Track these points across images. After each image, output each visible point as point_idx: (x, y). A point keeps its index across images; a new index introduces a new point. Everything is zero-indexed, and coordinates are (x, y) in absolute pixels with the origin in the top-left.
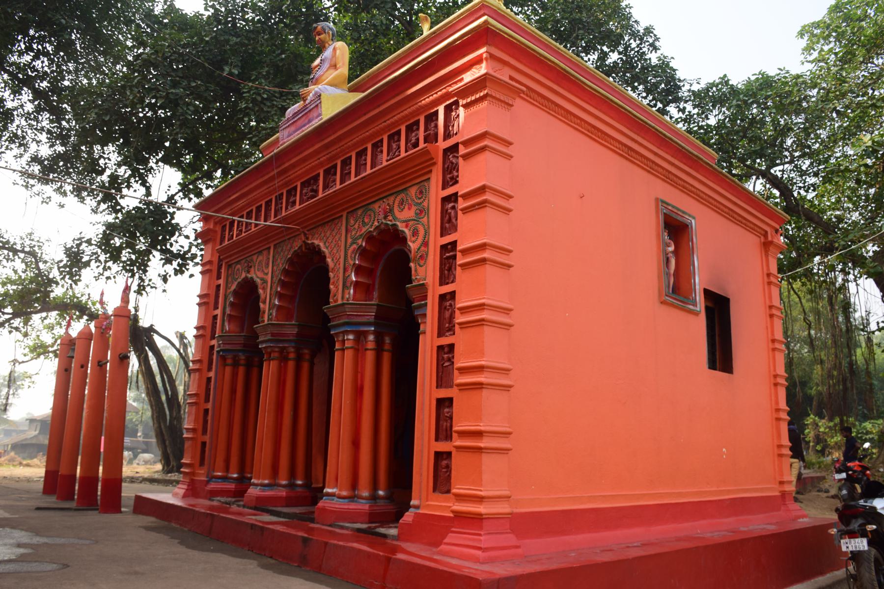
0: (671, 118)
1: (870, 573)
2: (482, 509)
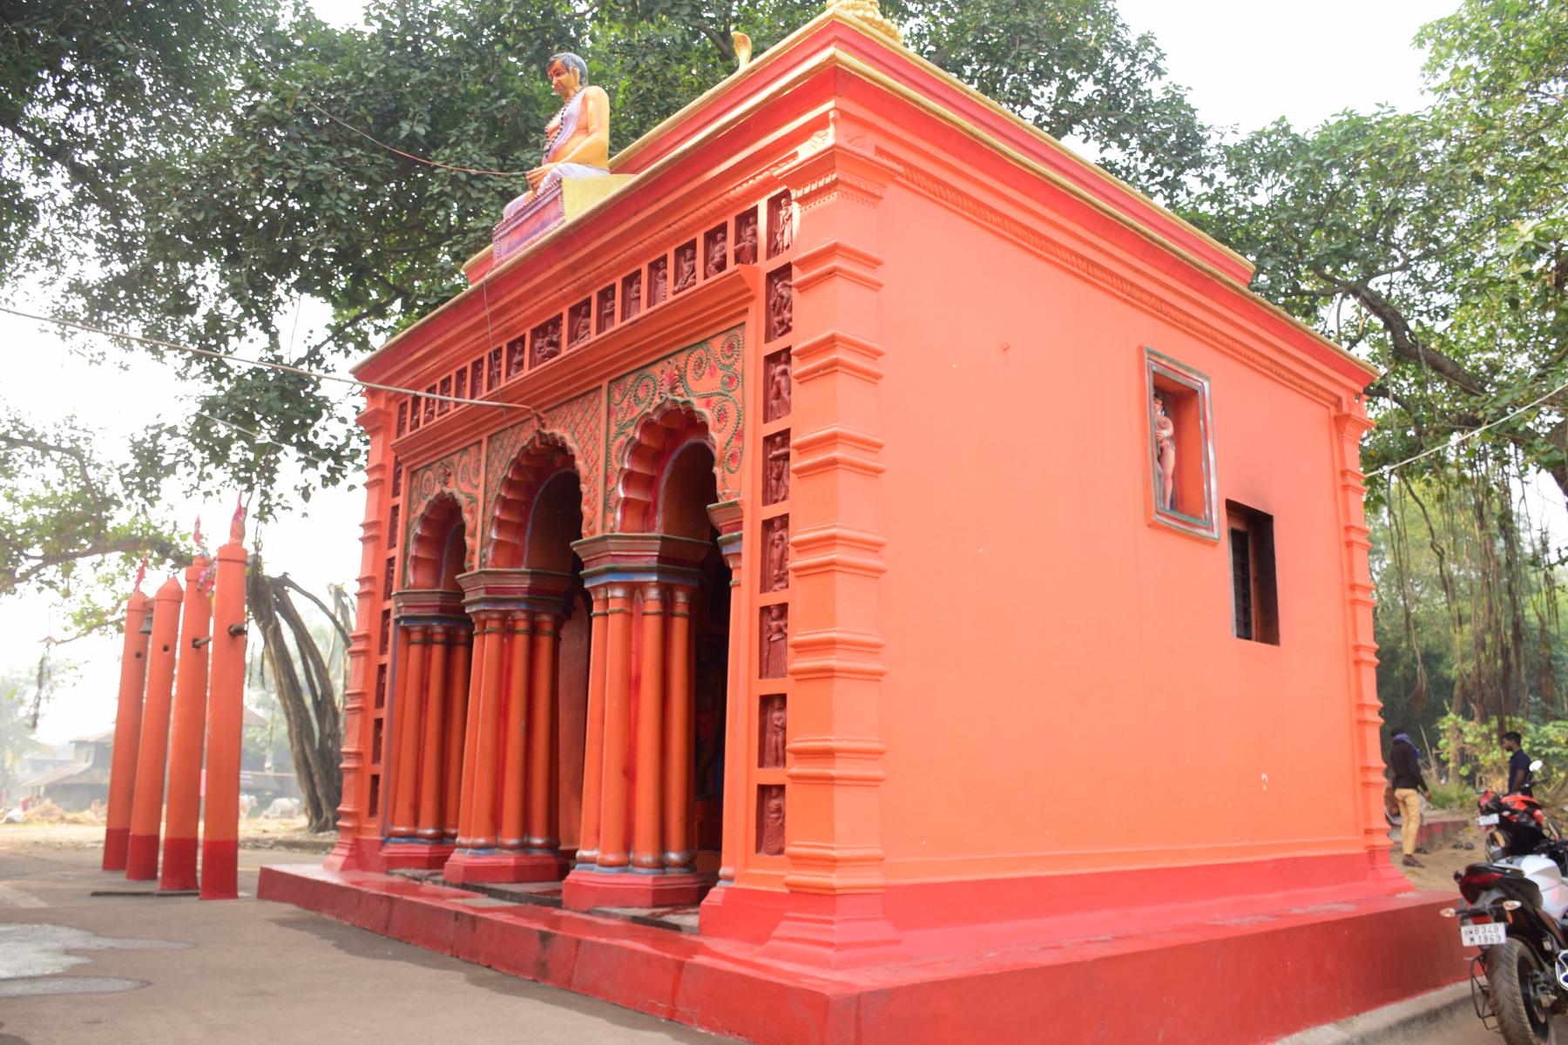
0: (1189, 194)
1: (1510, 982)
2: (835, 879)
